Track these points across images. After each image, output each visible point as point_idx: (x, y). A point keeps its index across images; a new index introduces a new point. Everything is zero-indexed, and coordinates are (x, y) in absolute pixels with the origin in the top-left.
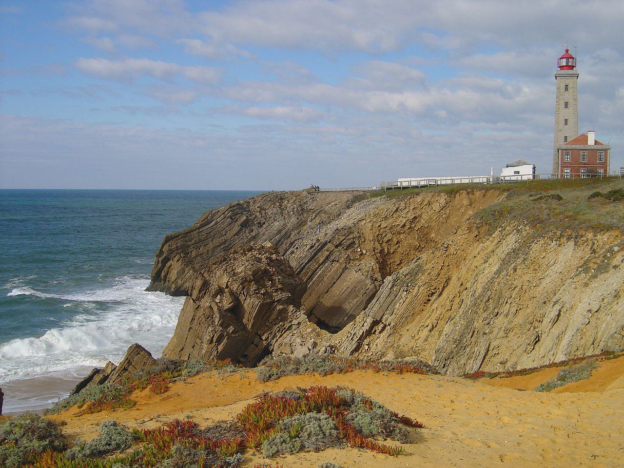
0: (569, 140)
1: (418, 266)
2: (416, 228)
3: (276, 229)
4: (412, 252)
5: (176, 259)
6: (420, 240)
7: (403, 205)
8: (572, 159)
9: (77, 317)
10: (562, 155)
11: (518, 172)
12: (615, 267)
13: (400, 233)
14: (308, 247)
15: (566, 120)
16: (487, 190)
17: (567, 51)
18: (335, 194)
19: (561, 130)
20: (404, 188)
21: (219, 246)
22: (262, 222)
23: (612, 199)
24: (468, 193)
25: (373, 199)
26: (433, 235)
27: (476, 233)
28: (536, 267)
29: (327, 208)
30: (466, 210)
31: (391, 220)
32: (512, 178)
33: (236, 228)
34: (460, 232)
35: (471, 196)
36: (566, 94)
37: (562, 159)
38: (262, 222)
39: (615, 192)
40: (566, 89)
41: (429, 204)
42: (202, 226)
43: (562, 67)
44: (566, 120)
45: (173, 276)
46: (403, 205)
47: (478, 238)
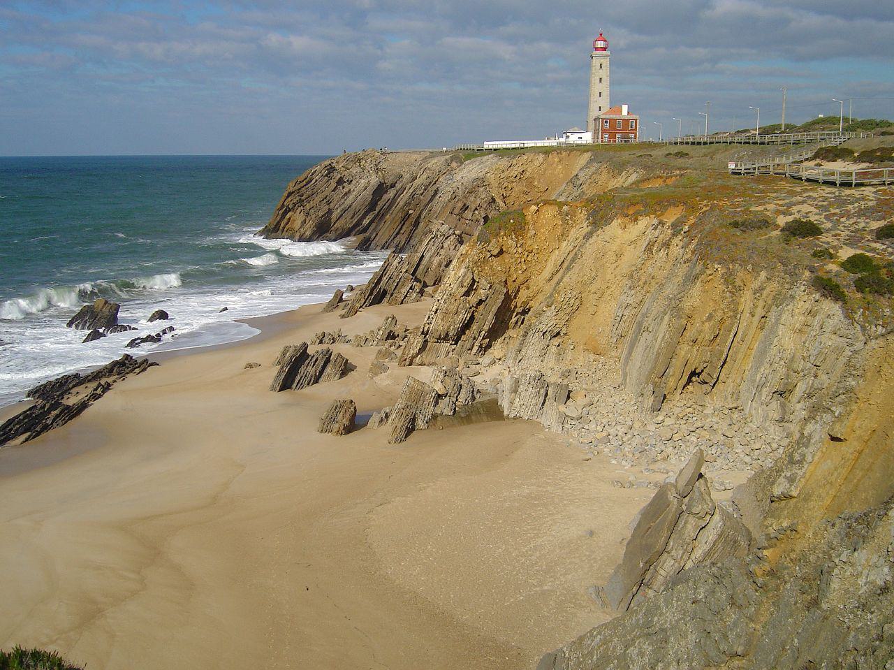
4: (521, 196)
5: (298, 211)
6: (527, 186)
9: (20, 301)
10: (602, 123)
11: (581, 138)
12: (352, 289)
14: (452, 192)
16: (571, 151)
18: (703, 150)
22: (350, 180)
23: (679, 156)
24: (558, 153)
26: (536, 183)
28: (776, 166)
31: (506, 173)
33: (333, 185)
36: (601, 71)
37: (602, 126)
45: (297, 224)
46: (515, 162)
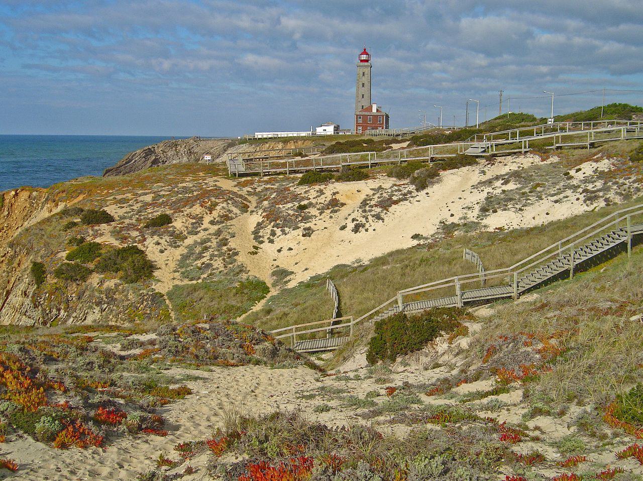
0: (364, 108)
7: (258, 148)
8: (363, 121)
17: (365, 50)
19: (360, 102)
20: (259, 139)
22: (164, 161)
25: (242, 145)
29: (211, 151)
32: (322, 134)
35: (296, 144)
38: (164, 161)
40: (363, 75)
42: (127, 163)
43: (362, 61)
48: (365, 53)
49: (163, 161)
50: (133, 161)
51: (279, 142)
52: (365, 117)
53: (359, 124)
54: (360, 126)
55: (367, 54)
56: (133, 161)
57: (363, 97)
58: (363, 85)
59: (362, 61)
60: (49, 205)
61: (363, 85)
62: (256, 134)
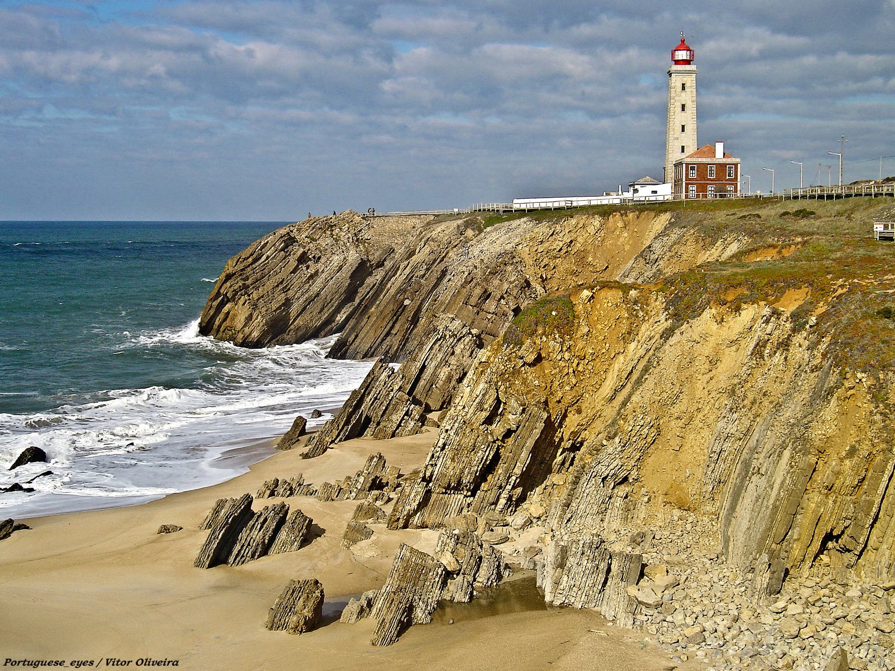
1: (658, 270)
2: (573, 252)
3: (336, 264)
13: (555, 257)
15: (683, 127)
17: (683, 41)
20: (555, 209)
21: (277, 286)
24: (622, 215)
26: (590, 259)
27: (702, 244)
30: (621, 232)
31: (546, 245)
32: (651, 199)
34: (688, 243)
36: (683, 94)
37: (687, 175)
39: (801, 211)
40: (683, 88)
41: (584, 226)
44: (683, 127)
46: (558, 228)
47: (704, 247)
48: (683, 46)
49: (314, 257)
50: (264, 257)
51: (594, 214)
52: (702, 167)
53: (690, 180)
54: (730, 184)
55: (688, 49)
56: (264, 257)
57: (683, 130)
58: (683, 107)
59: (677, 62)
60: (714, 311)
61: (683, 107)
62: (515, 201)
